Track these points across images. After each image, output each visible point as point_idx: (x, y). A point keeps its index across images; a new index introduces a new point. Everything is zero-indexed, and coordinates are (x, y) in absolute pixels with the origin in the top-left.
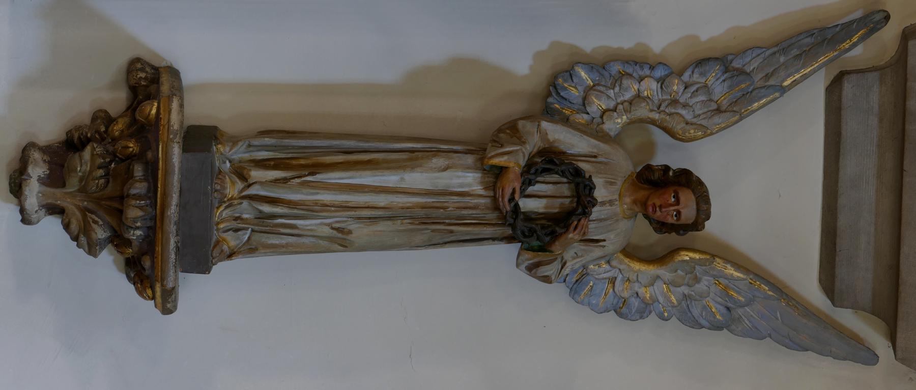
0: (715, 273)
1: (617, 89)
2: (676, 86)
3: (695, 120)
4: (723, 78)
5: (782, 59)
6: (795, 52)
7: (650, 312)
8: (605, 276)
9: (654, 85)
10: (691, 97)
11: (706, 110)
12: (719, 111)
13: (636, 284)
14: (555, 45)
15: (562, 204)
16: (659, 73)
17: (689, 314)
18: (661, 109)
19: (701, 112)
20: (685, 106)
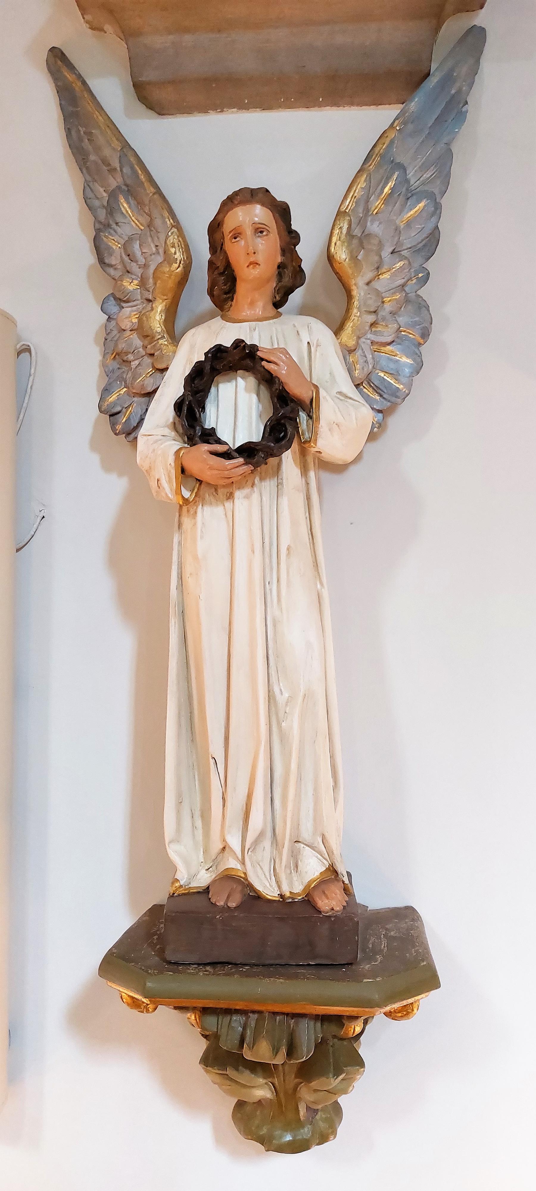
0: (361, 210)
1: (130, 357)
2: (131, 285)
3: (161, 251)
4: (114, 226)
5: (92, 157)
6: (86, 143)
7: (419, 296)
8: (369, 357)
9: (127, 311)
10: (136, 262)
11: (150, 239)
12: (150, 225)
13: (381, 313)
14: (95, 445)
15: (246, 389)
16: (113, 308)
17: (392, 135)
18: (151, 298)
19: (153, 246)
20: (146, 266)
